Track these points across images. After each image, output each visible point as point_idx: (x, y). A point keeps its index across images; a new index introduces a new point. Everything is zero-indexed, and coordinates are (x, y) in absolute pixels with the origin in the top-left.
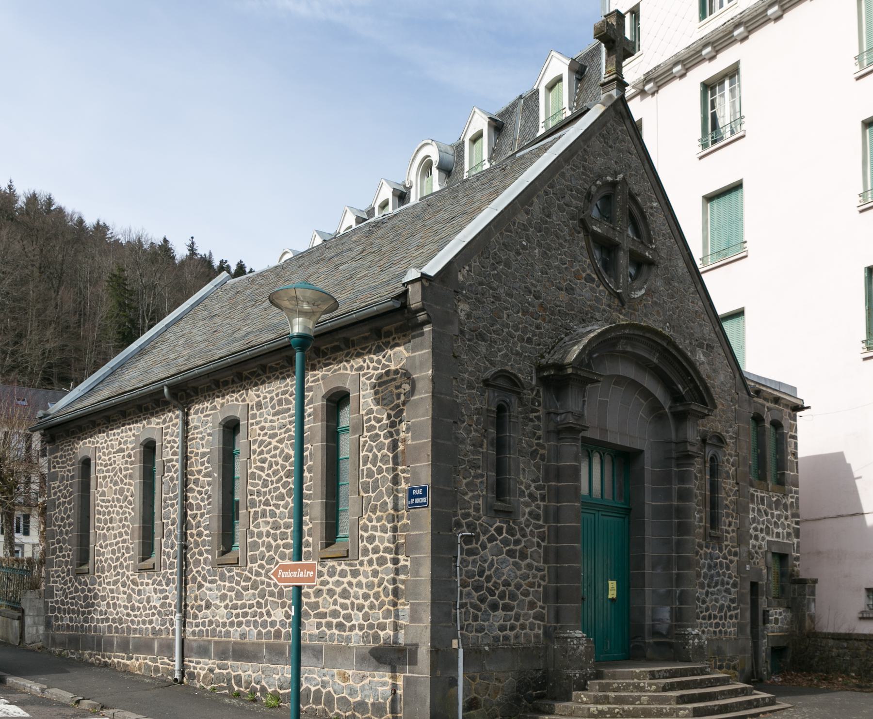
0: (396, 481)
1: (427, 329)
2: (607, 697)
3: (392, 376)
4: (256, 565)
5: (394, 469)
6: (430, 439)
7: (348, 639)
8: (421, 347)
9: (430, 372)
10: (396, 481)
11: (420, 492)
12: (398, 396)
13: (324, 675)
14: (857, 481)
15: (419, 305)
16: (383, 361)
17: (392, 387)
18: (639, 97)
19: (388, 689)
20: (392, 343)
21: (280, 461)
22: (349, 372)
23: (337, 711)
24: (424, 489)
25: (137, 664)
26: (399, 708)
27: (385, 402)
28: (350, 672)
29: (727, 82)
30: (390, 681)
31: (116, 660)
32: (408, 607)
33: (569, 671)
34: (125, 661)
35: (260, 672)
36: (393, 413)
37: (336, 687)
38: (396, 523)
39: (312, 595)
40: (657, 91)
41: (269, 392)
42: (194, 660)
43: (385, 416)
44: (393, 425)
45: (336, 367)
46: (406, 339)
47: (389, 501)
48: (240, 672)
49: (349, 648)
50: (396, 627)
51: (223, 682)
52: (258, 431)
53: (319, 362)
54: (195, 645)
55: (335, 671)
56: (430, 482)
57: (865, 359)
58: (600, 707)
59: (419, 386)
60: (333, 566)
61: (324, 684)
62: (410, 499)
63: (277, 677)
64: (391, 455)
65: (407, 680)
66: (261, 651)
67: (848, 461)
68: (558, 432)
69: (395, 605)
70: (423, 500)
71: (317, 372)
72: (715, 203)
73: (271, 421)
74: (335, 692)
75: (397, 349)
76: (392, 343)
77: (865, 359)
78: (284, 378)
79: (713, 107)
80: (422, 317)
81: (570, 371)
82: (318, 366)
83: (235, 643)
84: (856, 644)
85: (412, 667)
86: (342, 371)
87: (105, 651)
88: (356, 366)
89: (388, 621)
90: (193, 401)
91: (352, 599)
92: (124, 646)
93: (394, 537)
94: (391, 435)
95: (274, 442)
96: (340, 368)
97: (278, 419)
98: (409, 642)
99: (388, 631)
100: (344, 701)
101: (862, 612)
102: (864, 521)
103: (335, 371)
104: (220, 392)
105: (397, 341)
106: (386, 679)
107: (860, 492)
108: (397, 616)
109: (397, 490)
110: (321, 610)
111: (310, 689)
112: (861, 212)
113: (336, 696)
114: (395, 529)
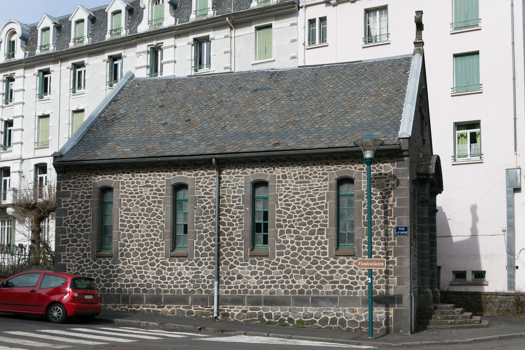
0: (386, 222)
1: (406, 159)
2: (448, 317)
3: (383, 176)
4: (283, 257)
5: (385, 218)
6: (408, 207)
7: (355, 293)
8: (403, 166)
9: (408, 178)
10: (386, 222)
11: (404, 229)
12: (388, 185)
13: (339, 310)
14: (448, 221)
15: (407, 149)
16: (377, 168)
17: (383, 180)
18: (324, 4)
19: (383, 315)
20: (382, 161)
21: (302, 206)
22: (353, 169)
23: (348, 327)
24: (406, 229)
25: (169, 310)
26: (390, 323)
27: (378, 187)
28: (358, 309)
29: (378, 13)
30: (385, 311)
31: (145, 309)
32: (396, 278)
33: (430, 307)
34: (156, 309)
35: (288, 311)
36: (384, 192)
37: (347, 316)
38: (386, 241)
39: (328, 273)
40: (337, 5)
41: (293, 171)
42: (229, 306)
43: (379, 193)
44: (384, 197)
45: (344, 166)
46: (392, 161)
47: (382, 232)
48: (270, 311)
49: (357, 297)
50: (387, 288)
51: (256, 317)
52: (284, 190)
53: (332, 162)
54: (229, 298)
55: (347, 308)
56: (409, 225)
57: (453, 165)
58: (451, 321)
59: (401, 183)
60: (344, 259)
61: (338, 315)
62: (397, 231)
63: (302, 313)
64: (383, 211)
65: (396, 311)
66: (290, 300)
67: (444, 211)
68: (422, 202)
69: (387, 277)
70: (405, 232)
71: (330, 166)
72: (262, 31)
73: (294, 186)
74: (346, 318)
75: (386, 164)
76: (382, 161)
77: (453, 165)
78: (305, 166)
79: (368, 23)
80: (405, 153)
81: (431, 177)
82: (330, 164)
83: (266, 297)
84: (465, 296)
85: (399, 305)
86: (348, 169)
87: (132, 303)
88: (358, 168)
89: (382, 285)
90: (225, 167)
91: (357, 274)
92: (156, 300)
93: (386, 247)
94: (383, 202)
95: (297, 197)
96: (347, 167)
97: (300, 186)
98: (396, 294)
99: (382, 289)
100: (354, 323)
101: (451, 282)
102: (452, 239)
103: (344, 168)
104: (251, 165)
105: (386, 161)
106: (382, 310)
107: (450, 226)
108: (388, 282)
109: (387, 227)
110: (335, 279)
111: (328, 318)
112: (452, 96)
113: (347, 320)
114: (386, 244)
